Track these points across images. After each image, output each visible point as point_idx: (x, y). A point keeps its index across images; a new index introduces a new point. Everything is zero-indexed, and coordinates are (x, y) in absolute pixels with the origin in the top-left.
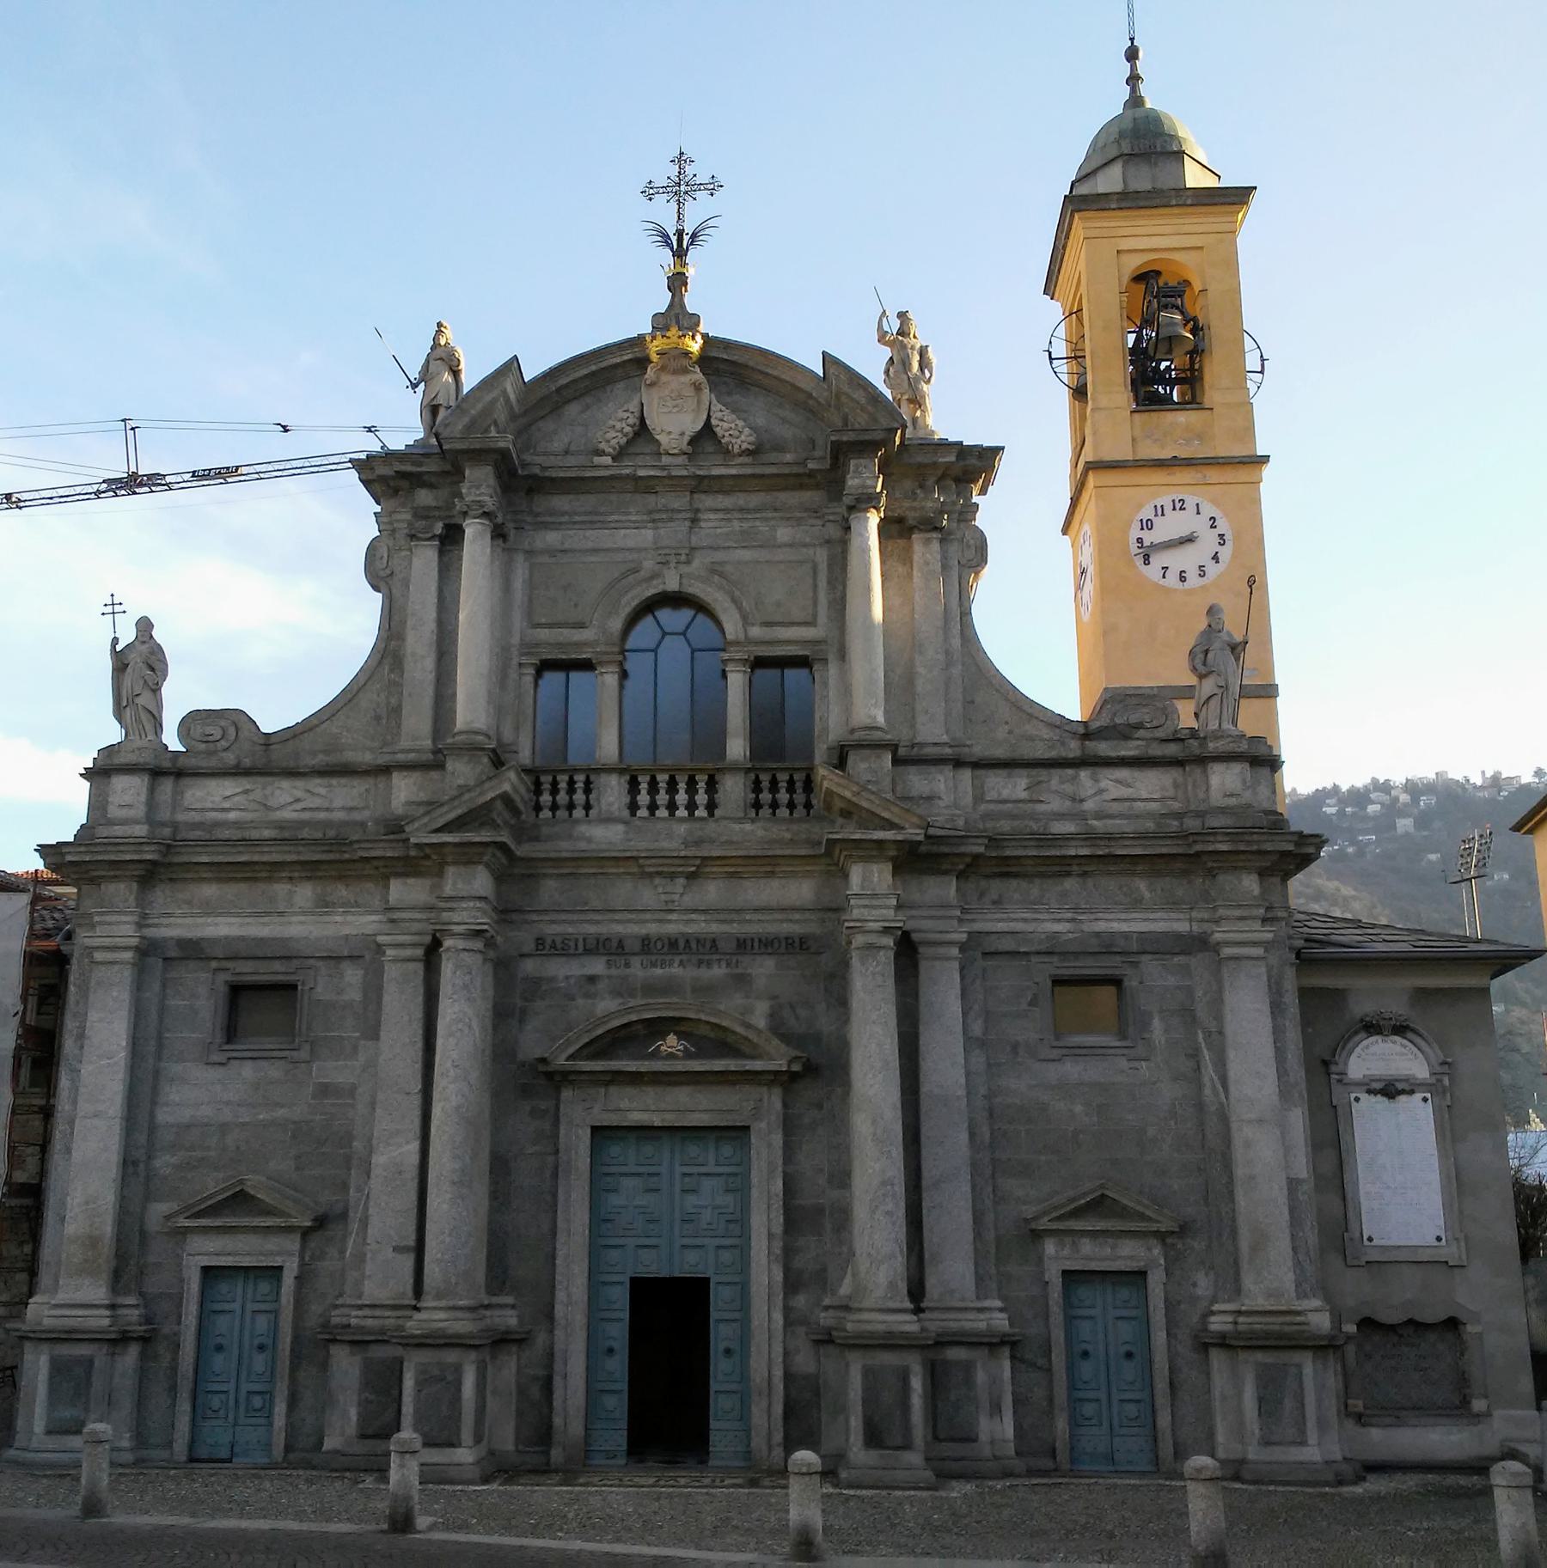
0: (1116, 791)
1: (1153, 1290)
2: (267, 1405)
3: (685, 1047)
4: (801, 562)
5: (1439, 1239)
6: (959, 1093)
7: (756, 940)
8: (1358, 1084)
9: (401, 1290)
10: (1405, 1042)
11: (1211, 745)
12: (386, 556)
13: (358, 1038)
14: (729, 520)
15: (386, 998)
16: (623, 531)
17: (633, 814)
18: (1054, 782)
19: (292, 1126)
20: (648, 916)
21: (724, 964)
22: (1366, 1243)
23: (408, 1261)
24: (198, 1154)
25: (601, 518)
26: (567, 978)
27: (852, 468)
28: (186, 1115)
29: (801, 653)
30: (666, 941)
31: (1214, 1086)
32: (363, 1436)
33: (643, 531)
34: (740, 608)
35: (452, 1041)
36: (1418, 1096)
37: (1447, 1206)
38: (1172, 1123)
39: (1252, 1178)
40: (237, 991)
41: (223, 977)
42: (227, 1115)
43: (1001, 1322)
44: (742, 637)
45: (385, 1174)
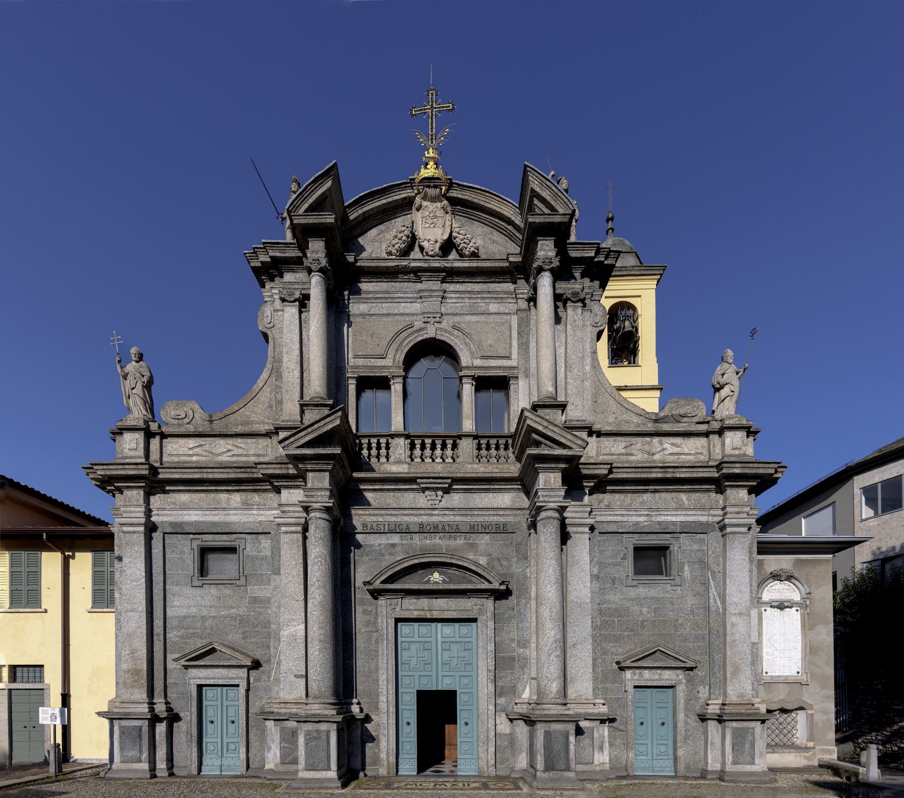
0: (670, 449)
1: (679, 694)
2: (237, 748)
3: (444, 579)
4: (503, 323)
5: (798, 673)
6: (587, 601)
7: (480, 525)
8: (766, 603)
9: (300, 695)
10: (790, 584)
11: (727, 422)
12: (270, 315)
13: (270, 574)
14: (463, 298)
15: (283, 553)
16: (403, 304)
17: (412, 460)
18: (639, 446)
19: (238, 618)
20: (422, 512)
21: (462, 538)
22: (764, 674)
23: (302, 682)
24: (191, 631)
25: (391, 295)
26: (380, 545)
27: (539, 246)
28: (183, 612)
29: (503, 374)
30: (432, 526)
31: (715, 598)
32: (282, 763)
33: (415, 304)
34: (470, 349)
35: (316, 567)
36: (794, 609)
37: (804, 658)
38: (691, 616)
39: (734, 641)
40: (204, 552)
41: (195, 544)
42: (205, 612)
43: (604, 709)
44: (470, 364)
45: (288, 640)
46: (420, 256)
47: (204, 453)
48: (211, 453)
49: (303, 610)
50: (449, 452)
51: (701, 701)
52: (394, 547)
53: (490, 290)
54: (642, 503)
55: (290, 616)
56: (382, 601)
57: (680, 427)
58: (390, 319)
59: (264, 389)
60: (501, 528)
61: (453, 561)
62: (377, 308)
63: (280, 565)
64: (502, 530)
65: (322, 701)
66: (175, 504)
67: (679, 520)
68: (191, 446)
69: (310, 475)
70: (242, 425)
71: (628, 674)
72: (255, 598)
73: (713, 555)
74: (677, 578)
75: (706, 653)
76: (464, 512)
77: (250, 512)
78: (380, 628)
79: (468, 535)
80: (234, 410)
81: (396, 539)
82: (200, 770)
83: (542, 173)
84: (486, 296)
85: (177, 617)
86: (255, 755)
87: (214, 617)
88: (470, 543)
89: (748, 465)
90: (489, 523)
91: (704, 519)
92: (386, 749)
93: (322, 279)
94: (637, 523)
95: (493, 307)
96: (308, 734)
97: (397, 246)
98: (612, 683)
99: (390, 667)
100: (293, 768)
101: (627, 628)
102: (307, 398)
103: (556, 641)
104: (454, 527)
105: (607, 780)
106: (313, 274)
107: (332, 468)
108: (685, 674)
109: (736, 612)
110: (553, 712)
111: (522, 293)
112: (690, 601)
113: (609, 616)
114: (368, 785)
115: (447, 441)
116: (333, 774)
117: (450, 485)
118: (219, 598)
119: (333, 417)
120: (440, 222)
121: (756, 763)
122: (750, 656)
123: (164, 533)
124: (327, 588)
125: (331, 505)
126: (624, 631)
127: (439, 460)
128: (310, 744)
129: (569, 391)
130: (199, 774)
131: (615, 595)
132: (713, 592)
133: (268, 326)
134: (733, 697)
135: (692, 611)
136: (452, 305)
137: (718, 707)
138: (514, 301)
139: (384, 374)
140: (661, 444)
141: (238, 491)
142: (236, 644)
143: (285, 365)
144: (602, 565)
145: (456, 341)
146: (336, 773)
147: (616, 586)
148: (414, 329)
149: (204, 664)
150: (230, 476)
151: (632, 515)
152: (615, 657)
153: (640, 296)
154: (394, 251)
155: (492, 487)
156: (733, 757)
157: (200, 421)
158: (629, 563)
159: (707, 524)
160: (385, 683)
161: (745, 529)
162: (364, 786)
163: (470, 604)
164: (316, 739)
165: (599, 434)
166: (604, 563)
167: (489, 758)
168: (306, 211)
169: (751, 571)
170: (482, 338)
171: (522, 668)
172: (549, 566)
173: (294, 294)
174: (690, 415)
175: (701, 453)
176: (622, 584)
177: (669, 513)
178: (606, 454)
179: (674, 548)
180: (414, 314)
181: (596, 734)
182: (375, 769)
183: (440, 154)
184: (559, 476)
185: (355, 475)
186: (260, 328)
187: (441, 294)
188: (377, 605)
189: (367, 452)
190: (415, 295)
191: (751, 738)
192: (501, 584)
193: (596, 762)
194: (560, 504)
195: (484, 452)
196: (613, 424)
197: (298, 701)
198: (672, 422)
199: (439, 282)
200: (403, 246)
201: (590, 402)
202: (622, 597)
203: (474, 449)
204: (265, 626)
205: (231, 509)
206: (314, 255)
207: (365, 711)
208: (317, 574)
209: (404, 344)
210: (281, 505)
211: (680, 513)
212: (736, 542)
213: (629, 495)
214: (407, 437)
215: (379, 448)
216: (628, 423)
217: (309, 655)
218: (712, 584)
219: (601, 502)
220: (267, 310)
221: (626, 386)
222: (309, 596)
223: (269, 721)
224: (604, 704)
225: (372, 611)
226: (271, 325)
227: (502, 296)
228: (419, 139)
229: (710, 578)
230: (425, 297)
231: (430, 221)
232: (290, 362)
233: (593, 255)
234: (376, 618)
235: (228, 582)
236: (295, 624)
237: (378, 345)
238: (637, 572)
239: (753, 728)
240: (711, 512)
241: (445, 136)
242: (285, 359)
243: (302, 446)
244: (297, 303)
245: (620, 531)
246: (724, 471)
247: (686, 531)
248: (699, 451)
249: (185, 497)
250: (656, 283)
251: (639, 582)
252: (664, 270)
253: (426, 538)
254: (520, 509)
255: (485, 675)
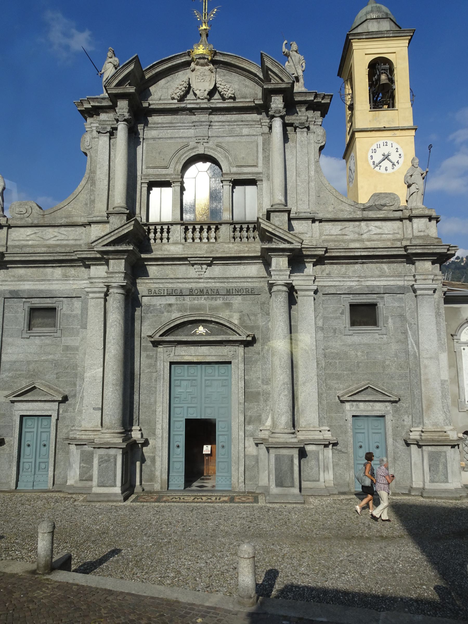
3: (206, 331)
7: (234, 289)
9: (96, 424)
11: (413, 212)
14: (224, 125)
15: (89, 313)
20: (192, 280)
26: (160, 304)
28: (14, 357)
29: (252, 178)
30: (199, 290)
31: (412, 345)
32: (81, 480)
33: (190, 130)
35: (113, 329)
38: (396, 359)
42: (30, 358)
43: (328, 435)
44: (228, 172)
46: (193, 97)
47: (38, 239)
48: (42, 238)
49: (102, 356)
50: (213, 234)
51: (406, 428)
52: (171, 306)
53: (243, 119)
54: (354, 271)
55: (92, 361)
56: (160, 349)
57: (381, 214)
58: (173, 141)
59: (82, 192)
60: (250, 291)
61: (213, 319)
62: (164, 134)
63: (87, 321)
64: (250, 292)
65: (112, 431)
66: (14, 276)
67: (382, 284)
68: (28, 234)
69: (111, 262)
70: (65, 218)
71: (347, 406)
72: (67, 346)
73: (409, 311)
74: (383, 328)
75: (408, 388)
76: (223, 280)
77: (68, 282)
78: (158, 370)
79: (226, 296)
80: (61, 207)
81: (172, 300)
82: (17, 486)
83: (272, 58)
84: (240, 123)
85: (9, 362)
86: (60, 473)
87: (36, 361)
88: (227, 303)
89: (426, 247)
90: (240, 288)
91: (401, 283)
92: (160, 468)
93: (125, 126)
94: (350, 287)
95: (245, 131)
96: (101, 457)
97: (178, 94)
98: (336, 413)
99: (165, 400)
100: (88, 484)
101: (346, 368)
102: (111, 210)
103: (284, 384)
104: (215, 292)
105: (329, 496)
106: (119, 123)
107: (127, 258)
108: (393, 405)
109: (428, 356)
110: (281, 440)
111: (265, 122)
112: (394, 347)
113: (332, 359)
114: (144, 498)
115: (211, 227)
116: (117, 490)
117: (212, 261)
118: (41, 347)
119: (128, 225)
120: (208, 78)
121: (450, 481)
122: (440, 392)
123: (5, 298)
124: (120, 344)
125: (125, 284)
126: (344, 371)
127: (205, 240)
128: (102, 465)
129: (298, 191)
130: (16, 488)
131: (336, 342)
132: (411, 340)
133: (88, 148)
134: (429, 426)
135: (396, 355)
136: (216, 129)
137: (418, 433)
138: (260, 126)
139: (167, 180)
140: (368, 227)
141: (60, 267)
142: (51, 382)
143: (98, 177)
144: (325, 319)
145: (219, 155)
146: (120, 489)
147: (337, 335)
148: (189, 147)
149: (27, 399)
150: (55, 258)
151: (346, 281)
152: (337, 392)
153: (395, 53)
154: (176, 97)
155: (242, 262)
156: (430, 477)
157: (36, 215)
158: (347, 317)
159: (403, 287)
160: (161, 413)
161: (432, 292)
162: (141, 500)
163: (226, 351)
164: (107, 461)
165: (321, 221)
166: (327, 317)
167: (240, 475)
168: (115, 86)
169: (438, 323)
170: (237, 153)
171: (266, 401)
172: (279, 326)
173: (106, 128)
174: (388, 205)
175: (398, 233)
176: (341, 333)
177: (374, 279)
178: (327, 235)
179: (380, 305)
180: (189, 137)
181: (321, 457)
182: (151, 485)
183: (210, 26)
184: (286, 259)
185: (143, 256)
186: (82, 150)
187: (208, 123)
188: (157, 351)
189: (154, 235)
190: (191, 125)
191: (444, 460)
192: (247, 337)
193: (322, 480)
194: (286, 282)
195: (238, 234)
196: (332, 213)
197: (95, 429)
198: (376, 210)
199: (208, 115)
200: (182, 93)
201: (314, 197)
202: (342, 344)
203: (231, 232)
204: (73, 368)
205: (54, 280)
206: (120, 110)
207: (145, 436)
208: (113, 334)
209: (182, 158)
210: (90, 278)
211: (382, 279)
212: (425, 302)
213: (344, 265)
214: (182, 224)
215: (162, 232)
216: (343, 211)
217: (104, 395)
218: (410, 333)
219: (323, 271)
220: (87, 137)
221: (385, 127)
222: (106, 350)
223: (72, 445)
224: (329, 431)
225: (153, 356)
226: (90, 147)
227: (251, 123)
228: (196, 16)
229: (408, 328)
230: (197, 126)
231: (201, 78)
232: (102, 184)
233: (313, 99)
234: (156, 361)
235: (48, 334)
236: (96, 367)
237: (164, 159)
238: (353, 323)
239: (445, 452)
240: (406, 278)
241: (214, 14)
242: (98, 172)
243: (107, 245)
244: (108, 134)
245: (338, 293)
246: (409, 251)
247: (388, 292)
248: (396, 232)
249: (22, 271)
250: (408, 42)
251: (355, 332)
252: (414, 33)
253: (194, 299)
254: (263, 277)
255: (237, 407)
